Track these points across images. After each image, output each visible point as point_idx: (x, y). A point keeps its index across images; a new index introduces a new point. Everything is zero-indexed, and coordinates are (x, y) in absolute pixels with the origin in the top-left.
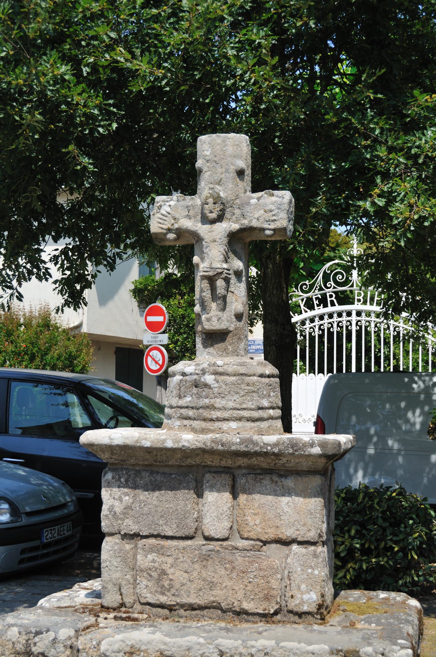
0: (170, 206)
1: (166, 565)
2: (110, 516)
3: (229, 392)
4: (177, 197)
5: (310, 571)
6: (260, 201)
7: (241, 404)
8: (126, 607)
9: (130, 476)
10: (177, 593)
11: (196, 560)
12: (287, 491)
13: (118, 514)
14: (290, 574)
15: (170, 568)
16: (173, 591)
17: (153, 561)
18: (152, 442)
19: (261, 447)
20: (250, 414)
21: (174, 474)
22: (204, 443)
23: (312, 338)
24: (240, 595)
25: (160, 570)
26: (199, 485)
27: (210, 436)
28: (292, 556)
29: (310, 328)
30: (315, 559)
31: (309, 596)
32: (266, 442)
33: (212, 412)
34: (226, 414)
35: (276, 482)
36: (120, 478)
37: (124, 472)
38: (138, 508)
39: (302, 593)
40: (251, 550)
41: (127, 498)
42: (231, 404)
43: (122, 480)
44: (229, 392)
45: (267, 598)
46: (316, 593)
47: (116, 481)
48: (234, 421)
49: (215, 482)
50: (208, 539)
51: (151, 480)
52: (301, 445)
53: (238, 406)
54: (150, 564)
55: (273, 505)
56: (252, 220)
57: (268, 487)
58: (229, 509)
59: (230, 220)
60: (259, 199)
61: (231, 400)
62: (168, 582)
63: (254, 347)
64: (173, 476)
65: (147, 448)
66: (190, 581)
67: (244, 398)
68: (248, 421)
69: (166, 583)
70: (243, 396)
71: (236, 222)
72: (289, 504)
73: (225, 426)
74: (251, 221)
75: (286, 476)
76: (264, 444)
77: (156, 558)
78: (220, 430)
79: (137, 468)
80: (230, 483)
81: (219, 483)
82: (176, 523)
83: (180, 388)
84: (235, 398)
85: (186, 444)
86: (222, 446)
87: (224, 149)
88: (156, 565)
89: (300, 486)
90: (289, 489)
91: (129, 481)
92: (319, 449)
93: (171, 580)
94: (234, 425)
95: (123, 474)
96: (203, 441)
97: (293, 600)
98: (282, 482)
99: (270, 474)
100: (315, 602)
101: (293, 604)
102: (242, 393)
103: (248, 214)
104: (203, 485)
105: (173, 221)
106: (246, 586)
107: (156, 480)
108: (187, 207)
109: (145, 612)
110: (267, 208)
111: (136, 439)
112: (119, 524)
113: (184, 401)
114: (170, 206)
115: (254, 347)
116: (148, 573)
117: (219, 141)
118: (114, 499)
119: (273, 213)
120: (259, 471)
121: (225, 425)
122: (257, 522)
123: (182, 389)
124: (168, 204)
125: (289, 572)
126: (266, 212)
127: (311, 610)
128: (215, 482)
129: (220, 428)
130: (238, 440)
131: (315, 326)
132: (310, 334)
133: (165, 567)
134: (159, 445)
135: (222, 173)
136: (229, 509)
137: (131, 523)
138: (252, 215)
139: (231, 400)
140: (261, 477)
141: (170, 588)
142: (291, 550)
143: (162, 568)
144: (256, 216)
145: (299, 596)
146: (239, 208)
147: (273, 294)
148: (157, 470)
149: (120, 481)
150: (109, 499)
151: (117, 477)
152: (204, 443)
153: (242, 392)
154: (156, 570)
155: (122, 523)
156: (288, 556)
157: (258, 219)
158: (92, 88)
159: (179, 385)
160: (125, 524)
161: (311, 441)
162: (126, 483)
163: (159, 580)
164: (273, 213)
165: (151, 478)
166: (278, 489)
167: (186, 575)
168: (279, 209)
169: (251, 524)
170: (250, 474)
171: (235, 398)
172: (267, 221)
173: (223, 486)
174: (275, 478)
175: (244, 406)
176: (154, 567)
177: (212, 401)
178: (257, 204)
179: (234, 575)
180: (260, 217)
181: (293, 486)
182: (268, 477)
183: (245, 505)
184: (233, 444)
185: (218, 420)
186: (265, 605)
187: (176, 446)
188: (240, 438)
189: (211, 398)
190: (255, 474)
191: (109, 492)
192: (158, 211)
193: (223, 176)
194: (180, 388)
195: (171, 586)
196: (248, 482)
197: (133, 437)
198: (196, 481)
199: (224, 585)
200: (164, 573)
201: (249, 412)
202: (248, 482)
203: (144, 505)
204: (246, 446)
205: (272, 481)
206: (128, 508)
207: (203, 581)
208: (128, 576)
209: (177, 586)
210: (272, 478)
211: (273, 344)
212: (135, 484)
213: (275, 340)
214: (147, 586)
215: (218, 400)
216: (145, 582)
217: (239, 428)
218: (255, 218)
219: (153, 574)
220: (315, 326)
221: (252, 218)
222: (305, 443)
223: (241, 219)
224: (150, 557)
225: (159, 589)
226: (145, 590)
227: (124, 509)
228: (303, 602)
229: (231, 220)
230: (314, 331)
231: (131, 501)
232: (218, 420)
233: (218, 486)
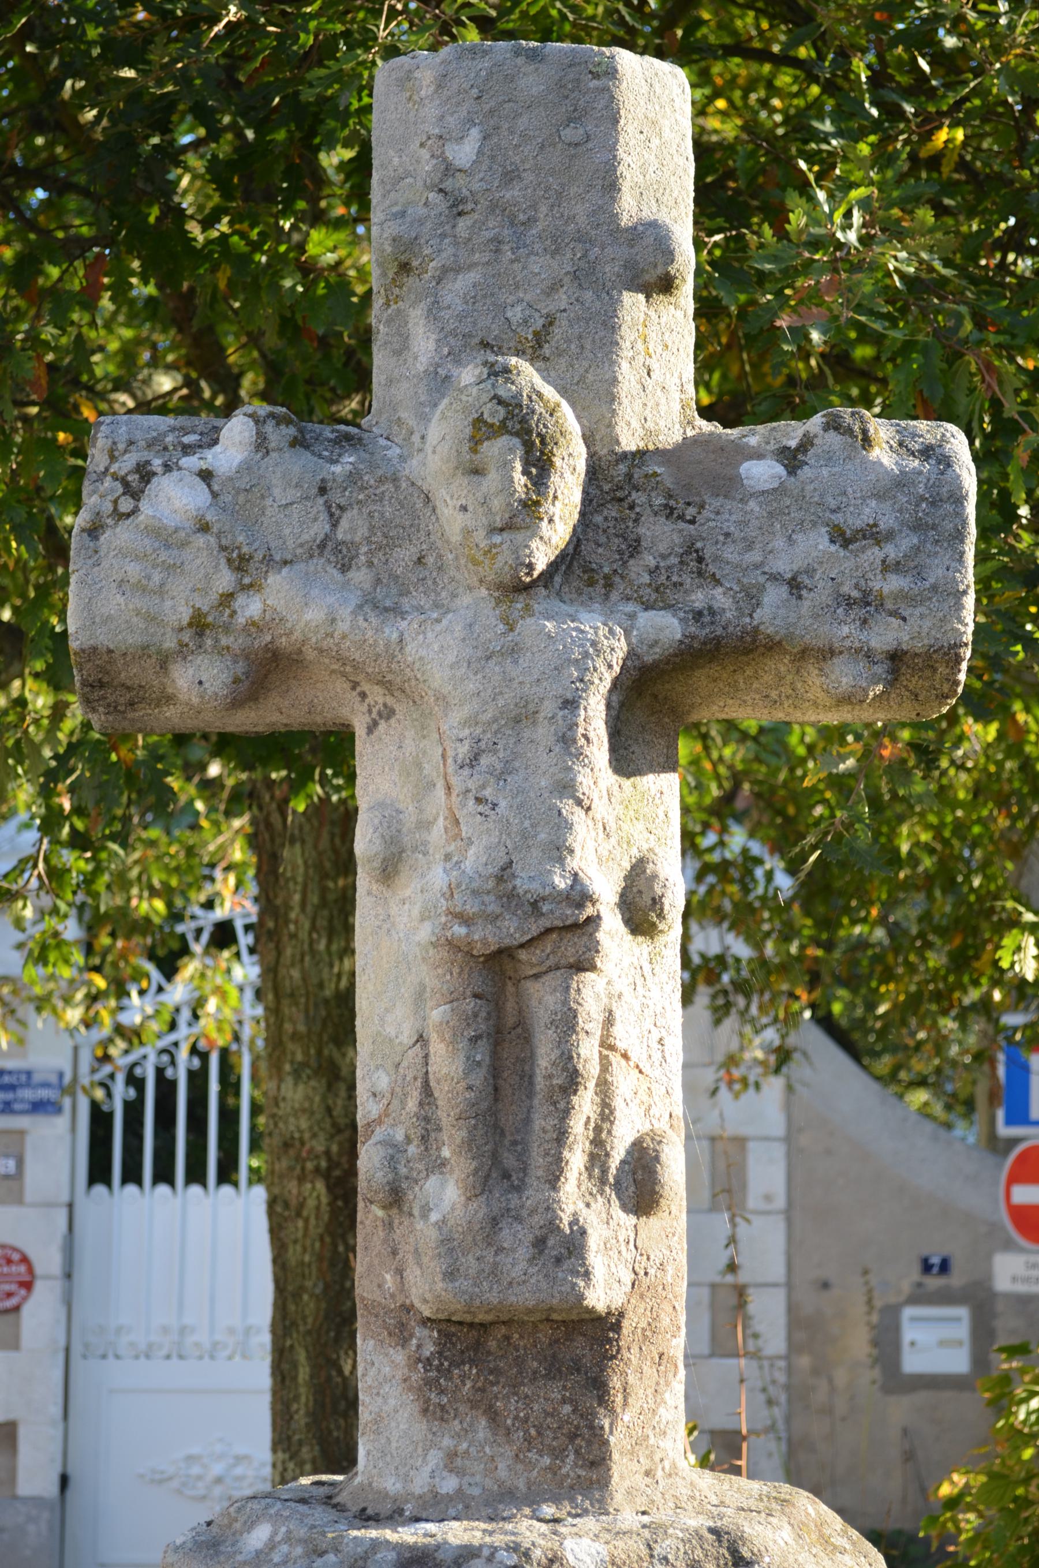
6: (805, 473)
23: (166, 1088)
56: (762, 588)
59: (609, 585)
74: (752, 597)
103: (730, 553)
105: (225, 580)
108: (323, 490)
110: (854, 521)
114: (206, 476)
124: (191, 462)
126: (846, 543)
131: (176, 1044)
132: (160, 1072)
135: (554, 287)
144: (783, 565)
146: (669, 512)
147: (313, 952)
157: (795, 585)
164: (892, 551)
168: (918, 526)
178: (780, 491)
180: (810, 572)
193: (561, 299)
211: (317, 1170)
213: (327, 1153)
218: (775, 578)
220: (176, 1044)
221: (756, 578)
229: (620, 585)
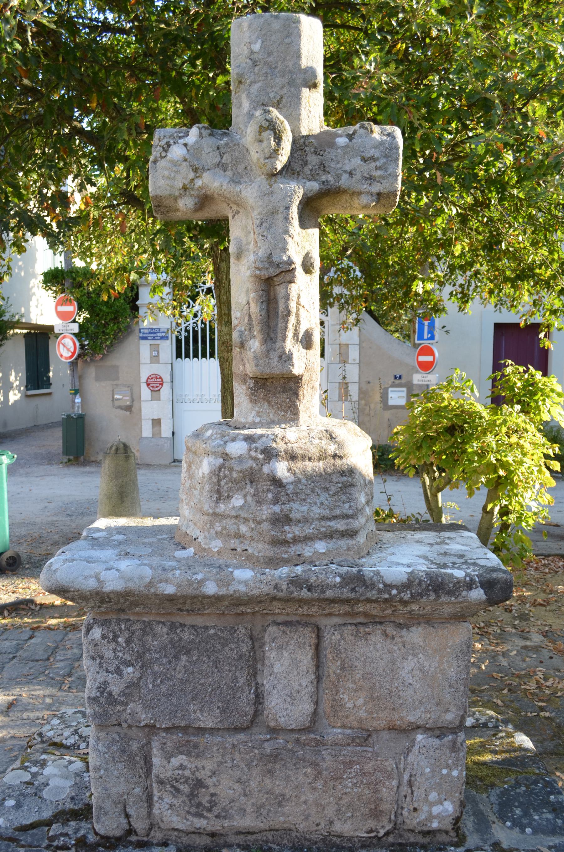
0: (185, 145)
1: (203, 772)
2: (102, 700)
3: (313, 491)
4: (200, 129)
5: (445, 771)
7: (331, 509)
8: (137, 835)
9: (133, 633)
10: (223, 814)
11: (254, 764)
12: (411, 652)
13: (116, 697)
14: (413, 779)
15: (211, 777)
16: (216, 811)
17: (181, 767)
18: (179, 586)
19: (380, 591)
20: (347, 524)
21: (214, 627)
22: (276, 586)
24: (330, 812)
25: (193, 780)
26: (257, 645)
27: (284, 571)
28: (415, 749)
29: (194, 323)
30: (453, 754)
31: (441, 808)
32: (388, 582)
33: (287, 528)
34: (309, 530)
35: (393, 638)
36: (116, 637)
37: (123, 626)
38: (150, 686)
39: (432, 805)
40: (348, 745)
41: (130, 669)
42: (317, 511)
43: (120, 640)
44: (313, 491)
45: (376, 814)
46: (453, 802)
47: (108, 642)
48: (320, 539)
49: (286, 640)
50: (275, 731)
51: (172, 640)
52: (451, 585)
53: (327, 513)
54: (176, 772)
55: (387, 675)
57: (379, 646)
58: (312, 683)
59: (299, 174)
60: (350, 137)
61: (316, 503)
62: (207, 798)
63: (159, 334)
64: (212, 632)
65: (169, 595)
66: (245, 795)
67: (336, 497)
68: (343, 536)
69: (205, 800)
70: (335, 494)
71: (313, 177)
72: (414, 672)
73: (307, 551)
74: (339, 177)
75: (407, 627)
76: (385, 585)
77: (185, 763)
78: (299, 560)
79: (144, 619)
80: (314, 641)
81: (293, 642)
82: (218, 708)
83: (219, 481)
84: (322, 499)
85: (242, 588)
86: (309, 590)
87: (287, 41)
88: (187, 773)
89: (433, 643)
90: (413, 649)
91: (133, 641)
92: (482, 591)
93: (212, 795)
94: (321, 546)
95: (121, 630)
96: (273, 583)
97: (415, 814)
98: (402, 637)
99: (381, 623)
100: (450, 816)
101: (415, 822)
102: (333, 489)
103: (333, 165)
104: (264, 644)
105: (192, 175)
106: (340, 799)
107: (181, 639)
108: (218, 148)
109: (170, 842)
111: (148, 580)
112: (119, 712)
113: (231, 506)
114: (185, 145)
115: (159, 334)
116: (172, 786)
117: (276, 25)
118: (107, 671)
119: (378, 164)
120: (361, 620)
121: (308, 548)
122: (360, 702)
123: (222, 483)
125: (411, 776)
127: (444, 828)
128: (286, 640)
129: (299, 555)
130: (338, 579)
132: (194, 328)
133: (201, 775)
134: (190, 591)
135: (282, 87)
136: (312, 683)
137: (139, 709)
138: (340, 166)
139: (316, 503)
140: (367, 630)
141: (211, 807)
142: (414, 740)
143: (197, 779)
144: (348, 168)
145: (426, 808)
146: (316, 153)
148: (181, 621)
149: (117, 642)
150: (98, 672)
151: (111, 635)
152: (276, 586)
153: (332, 488)
154: (186, 782)
155: (124, 710)
156: (409, 750)
157: (351, 174)
158: (104, 623)
159: (218, 475)
160: (129, 711)
161: (468, 579)
162: (127, 645)
163: (192, 796)
164: (378, 164)
165: (172, 636)
166: (396, 648)
167: (237, 786)
169: (350, 705)
170: (345, 624)
171: (322, 499)
172: (366, 179)
173: (300, 647)
174: (391, 630)
175: (338, 512)
176: (183, 776)
177: (286, 507)
178: (347, 146)
179: (319, 784)
180: (355, 170)
181: (421, 644)
182: (378, 630)
183: (338, 676)
184: (329, 587)
185: (296, 540)
186: (371, 824)
187: (223, 592)
188: (340, 576)
189: (284, 504)
190: (356, 625)
191: (98, 661)
192: (164, 154)
194: (219, 481)
195: (213, 804)
196: (344, 639)
197: (141, 578)
198: (251, 638)
199: (303, 798)
200: (199, 784)
201: (345, 521)
202: (344, 639)
203: (161, 682)
204: (353, 590)
205: (386, 635)
206: (133, 685)
207: (267, 793)
208: (137, 790)
209: (224, 802)
210: (385, 631)
212: (144, 646)
214: (171, 806)
215: (295, 506)
216: (168, 799)
217: (329, 551)
218: (345, 172)
219: (181, 787)
221: (340, 172)
222: (458, 582)
223: (321, 173)
224: (175, 761)
225: (193, 810)
226: (169, 811)
227: (127, 687)
228: (431, 817)
229: (302, 175)
230: (197, 326)
231: (138, 674)
232: (296, 540)
233: (291, 647)
